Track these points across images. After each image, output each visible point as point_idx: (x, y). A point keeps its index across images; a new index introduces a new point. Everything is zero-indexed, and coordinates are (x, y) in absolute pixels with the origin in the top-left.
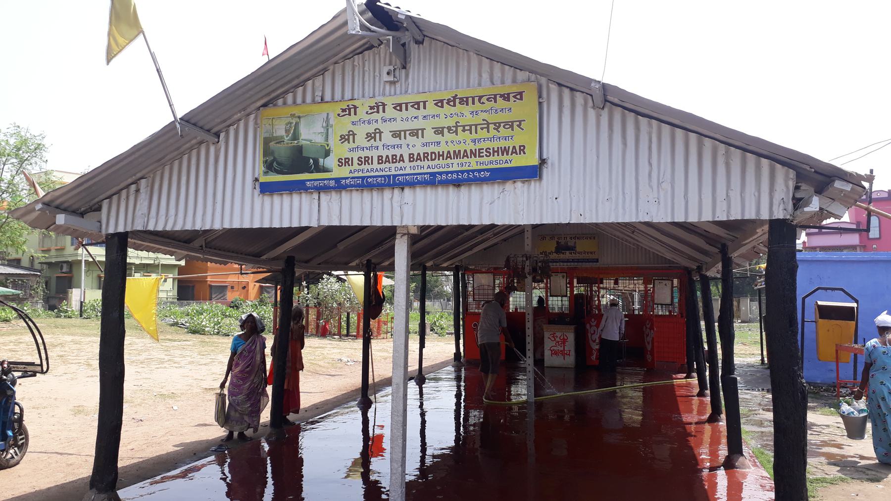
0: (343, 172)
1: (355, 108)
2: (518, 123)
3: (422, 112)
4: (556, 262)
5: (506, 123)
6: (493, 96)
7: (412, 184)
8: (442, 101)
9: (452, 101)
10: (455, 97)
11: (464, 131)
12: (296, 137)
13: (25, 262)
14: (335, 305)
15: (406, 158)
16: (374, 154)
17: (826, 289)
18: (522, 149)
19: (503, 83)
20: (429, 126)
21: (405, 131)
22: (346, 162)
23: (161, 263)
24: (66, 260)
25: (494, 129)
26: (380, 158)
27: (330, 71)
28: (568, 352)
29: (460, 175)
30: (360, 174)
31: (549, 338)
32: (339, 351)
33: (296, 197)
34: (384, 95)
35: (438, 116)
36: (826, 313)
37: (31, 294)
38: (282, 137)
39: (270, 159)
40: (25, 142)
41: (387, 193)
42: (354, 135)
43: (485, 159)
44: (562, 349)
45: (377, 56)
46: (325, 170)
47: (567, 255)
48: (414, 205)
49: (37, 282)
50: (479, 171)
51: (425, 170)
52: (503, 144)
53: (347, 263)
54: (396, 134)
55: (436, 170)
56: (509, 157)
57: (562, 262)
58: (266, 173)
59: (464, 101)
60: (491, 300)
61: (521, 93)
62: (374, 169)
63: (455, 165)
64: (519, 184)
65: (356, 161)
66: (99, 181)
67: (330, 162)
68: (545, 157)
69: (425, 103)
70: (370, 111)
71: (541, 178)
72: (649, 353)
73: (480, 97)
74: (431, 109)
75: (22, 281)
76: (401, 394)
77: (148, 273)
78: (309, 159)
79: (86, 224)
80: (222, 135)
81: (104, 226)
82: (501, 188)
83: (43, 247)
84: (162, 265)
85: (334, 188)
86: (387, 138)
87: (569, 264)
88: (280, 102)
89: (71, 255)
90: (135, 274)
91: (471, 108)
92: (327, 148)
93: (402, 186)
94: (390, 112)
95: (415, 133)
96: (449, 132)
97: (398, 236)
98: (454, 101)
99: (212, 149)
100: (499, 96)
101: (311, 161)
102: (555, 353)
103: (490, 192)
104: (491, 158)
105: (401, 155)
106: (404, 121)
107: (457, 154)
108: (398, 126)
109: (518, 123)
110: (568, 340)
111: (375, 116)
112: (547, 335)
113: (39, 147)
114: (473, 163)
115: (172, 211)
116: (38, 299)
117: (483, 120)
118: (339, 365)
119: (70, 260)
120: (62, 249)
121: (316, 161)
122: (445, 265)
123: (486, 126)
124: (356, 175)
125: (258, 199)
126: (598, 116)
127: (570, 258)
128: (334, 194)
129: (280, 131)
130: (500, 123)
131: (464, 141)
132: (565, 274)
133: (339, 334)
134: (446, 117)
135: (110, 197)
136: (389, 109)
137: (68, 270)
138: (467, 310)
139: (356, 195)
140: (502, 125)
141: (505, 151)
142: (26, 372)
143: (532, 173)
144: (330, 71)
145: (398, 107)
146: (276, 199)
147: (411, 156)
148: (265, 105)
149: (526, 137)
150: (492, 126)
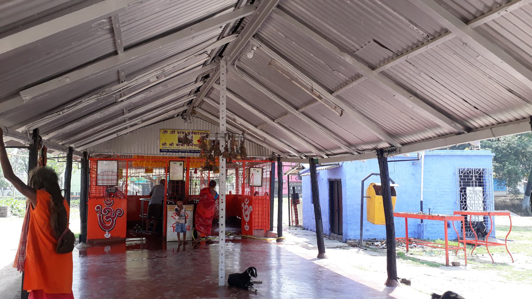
4: (176, 152)
19: (247, 23)
28: (188, 227)
31: (172, 216)
47: (185, 147)
60: (114, 184)
66: (293, 114)
72: (246, 223)
110: (188, 218)
127: (188, 149)
132: (182, 163)
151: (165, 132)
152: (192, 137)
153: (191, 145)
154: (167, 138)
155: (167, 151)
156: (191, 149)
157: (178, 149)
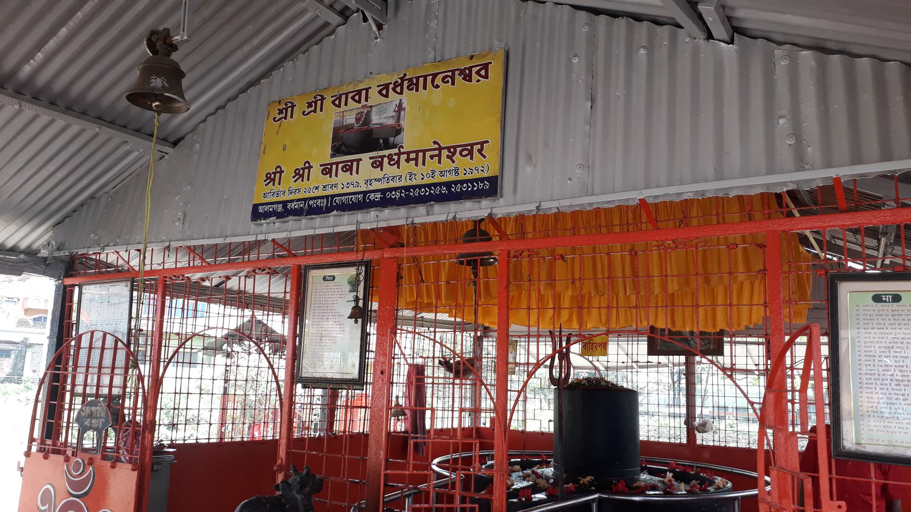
2: (479, 146)
6: (450, 74)
8: (386, 86)
25: (448, 157)
29: (432, 190)
70: (307, 110)
78: (379, 140)
92: (398, 128)
96: (389, 163)
98: (402, 85)
100: (459, 72)
101: (381, 140)
109: (479, 146)
117: (435, 143)
121: (386, 141)
123: (437, 152)
127: (376, 186)
130: (455, 147)
140: (459, 150)
151: (286, 110)
152: (400, 108)
153: (390, 157)
154: (287, 142)
155: (280, 208)
156: (392, 184)
157: (330, 192)
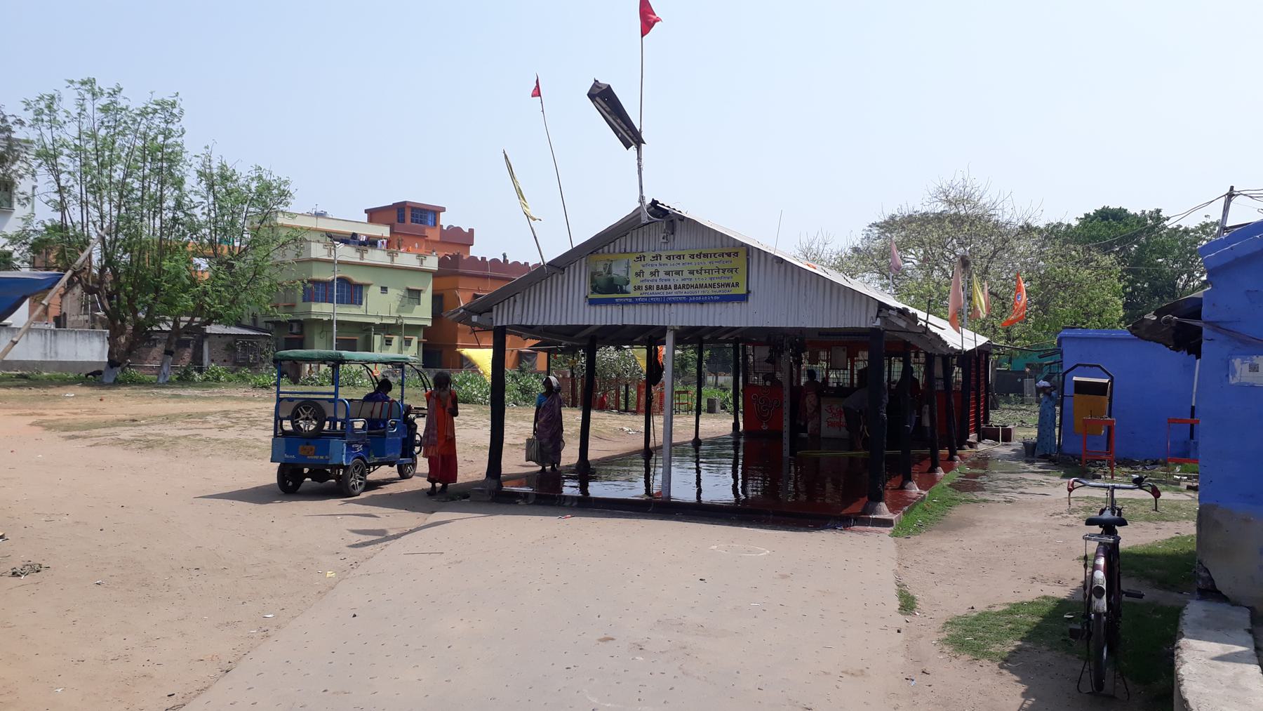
0: (637, 294)
1: (644, 257)
3: (682, 261)
5: (729, 269)
7: (676, 302)
9: (699, 256)
10: (701, 253)
11: (705, 272)
12: (609, 272)
13: (247, 321)
14: (614, 376)
15: (673, 288)
16: (655, 284)
17: (1085, 366)
18: (737, 284)
20: (686, 269)
21: (672, 272)
22: (639, 288)
23: (404, 323)
24: (297, 318)
26: (658, 286)
27: (630, 234)
30: (647, 295)
32: (619, 422)
33: (609, 308)
34: (661, 250)
35: (691, 263)
36: (1080, 387)
37: (261, 358)
38: (602, 272)
39: (595, 285)
40: (268, 187)
41: (662, 307)
42: (643, 272)
43: (717, 289)
44: (838, 420)
45: (657, 228)
46: (627, 292)
48: (677, 314)
49: (268, 345)
50: (713, 296)
51: (684, 294)
52: (727, 281)
53: (632, 339)
54: (667, 273)
55: (689, 294)
56: (730, 289)
57: (844, 335)
58: (592, 293)
59: (706, 256)
61: (737, 253)
62: (655, 293)
63: (700, 292)
64: (736, 304)
65: (644, 288)
67: (630, 288)
68: (750, 289)
69: (684, 256)
71: (747, 300)
73: (715, 254)
74: (687, 259)
75: (252, 343)
76: (669, 422)
77: (390, 335)
79: (484, 320)
80: (566, 269)
81: (494, 322)
82: (726, 305)
83: (285, 302)
84: (406, 325)
85: (631, 303)
86: (662, 275)
87: (850, 337)
88: (601, 251)
89: (302, 314)
90: (375, 336)
91: (709, 260)
93: (670, 303)
94: (664, 260)
95: (678, 273)
97: (668, 331)
99: (560, 277)
102: (831, 425)
103: (719, 308)
104: (720, 289)
105: (670, 286)
106: (672, 265)
107: (701, 286)
108: (668, 268)
111: (655, 262)
112: (824, 407)
113: (284, 194)
114: (710, 291)
115: (536, 314)
116: (268, 364)
118: (621, 433)
119: (302, 319)
120: (293, 306)
121: (621, 287)
122: (724, 338)
124: (644, 296)
125: (587, 308)
126: (779, 267)
128: (631, 306)
129: (600, 268)
131: (705, 279)
132: (846, 348)
133: (617, 407)
134: (696, 264)
135: (498, 304)
136: (664, 258)
137: (299, 331)
138: (747, 381)
139: (644, 307)
141: (728, 285)
142: (418, 414)
143: (743, 298)
144: (630, 234)
145: (669, 257)
146: (598, 308)
147: (675, 286)
148: (592, 253)
149: (740, 278)
150: (721, 271)
